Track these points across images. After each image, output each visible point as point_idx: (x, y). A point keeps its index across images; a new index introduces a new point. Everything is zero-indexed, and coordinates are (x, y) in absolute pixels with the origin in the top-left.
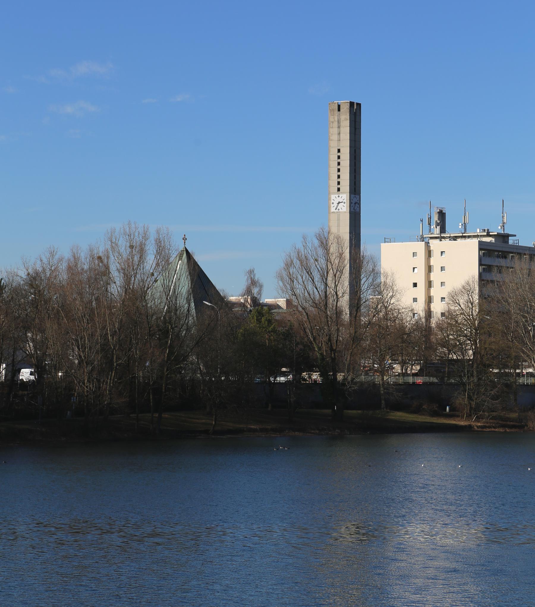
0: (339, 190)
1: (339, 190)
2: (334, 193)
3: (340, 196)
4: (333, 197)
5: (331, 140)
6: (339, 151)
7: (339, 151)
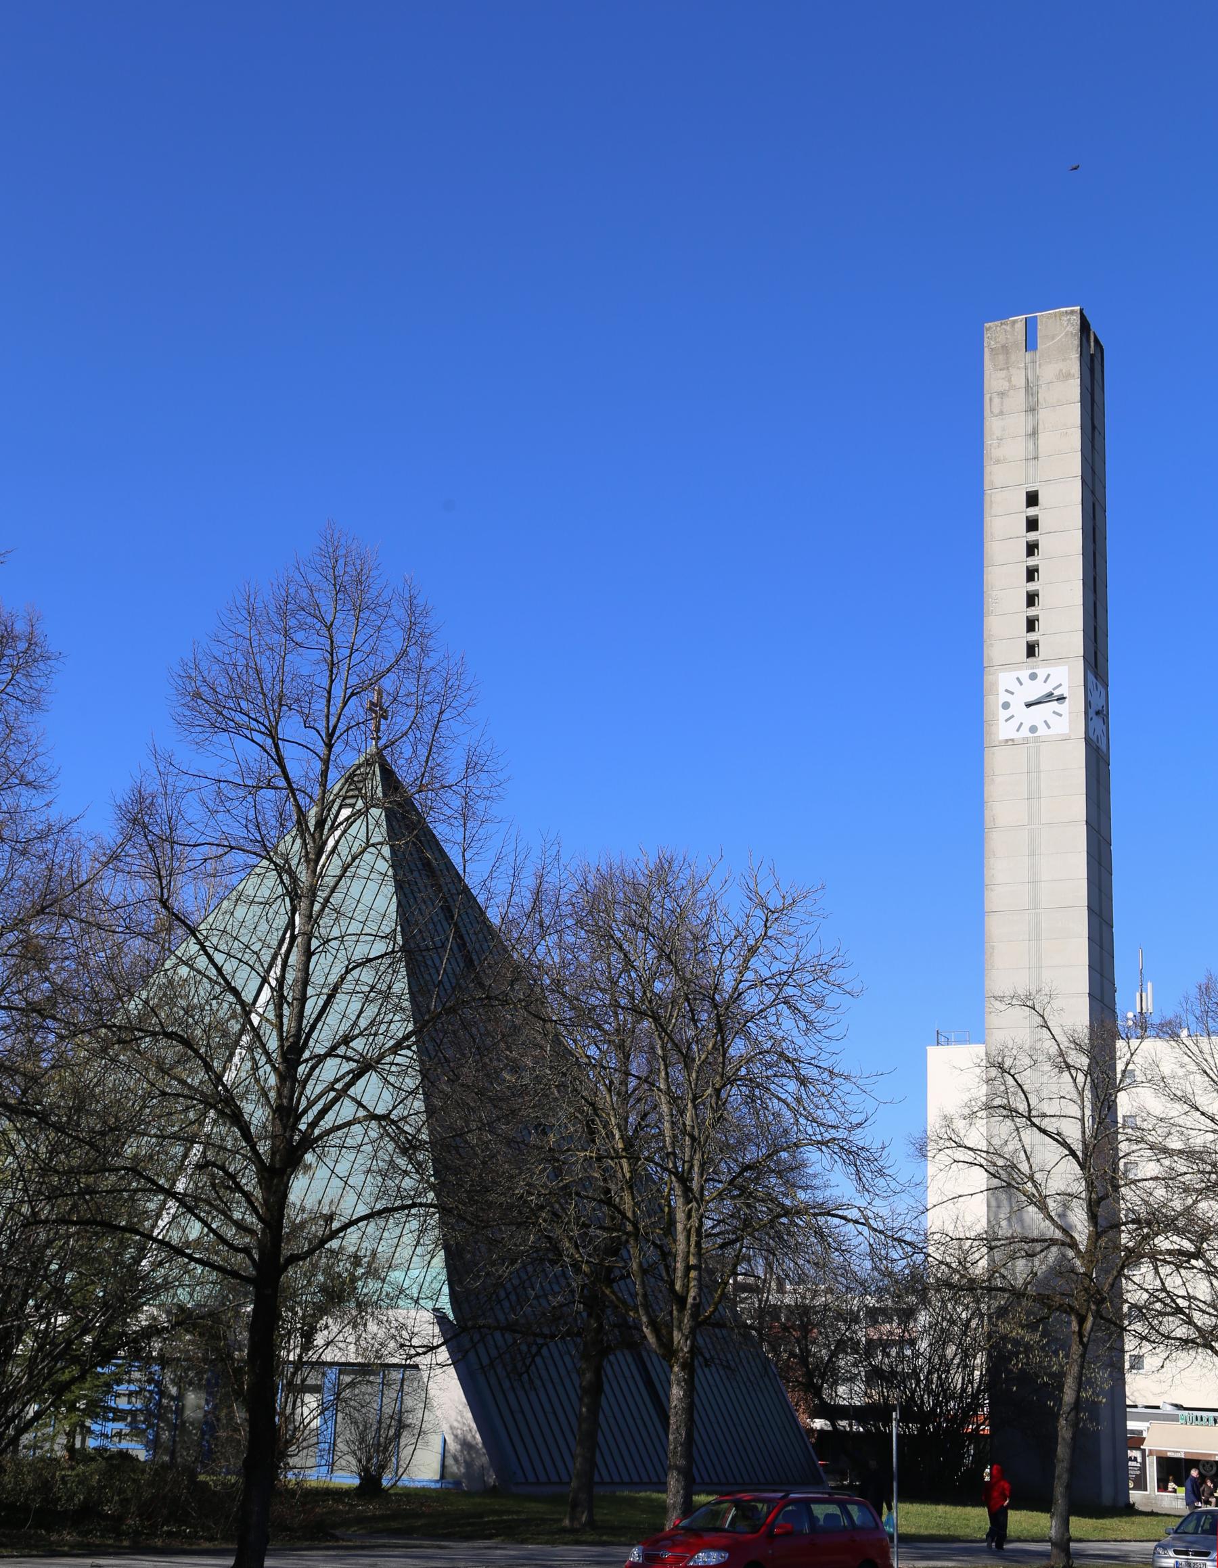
1: (1031, 650)
3: (1042, 673)
5: (998, 461)
6: (1032, 499)
7: (1032, 499)
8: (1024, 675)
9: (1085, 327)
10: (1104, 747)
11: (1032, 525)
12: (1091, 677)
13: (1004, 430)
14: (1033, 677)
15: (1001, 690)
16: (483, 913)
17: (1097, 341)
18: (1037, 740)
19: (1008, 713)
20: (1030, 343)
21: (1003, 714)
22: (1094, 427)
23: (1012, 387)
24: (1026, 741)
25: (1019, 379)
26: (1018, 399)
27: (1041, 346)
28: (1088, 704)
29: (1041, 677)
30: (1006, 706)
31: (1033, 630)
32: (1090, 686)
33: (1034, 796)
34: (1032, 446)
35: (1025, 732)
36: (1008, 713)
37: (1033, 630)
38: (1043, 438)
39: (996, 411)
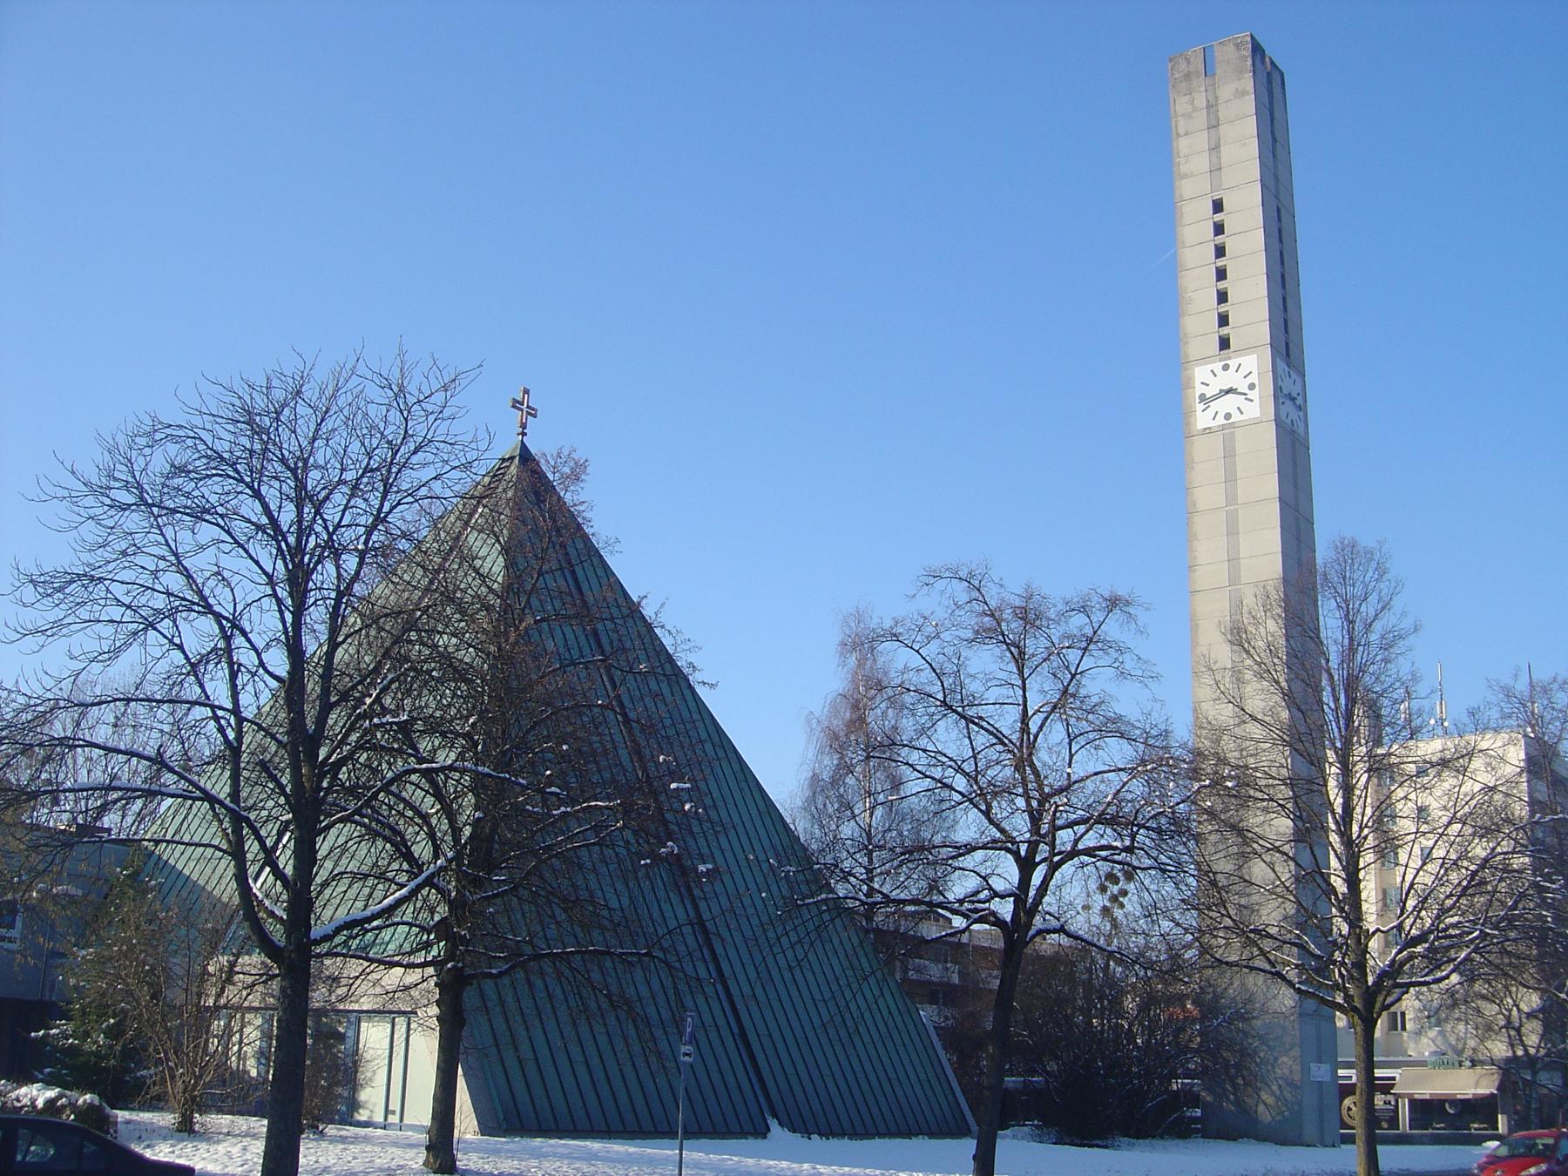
0: (1224, 343)
1: (1224, 343)
2: (1204, 360)
3: (1233, 363)
4: (1201, 373)
5: (1186, 176)
6: (1218, 206)
7: (1218, 206)
8: (1218, 367)
9: (1257, 49)
10: (1301, 430)
11: (1220, 251)
12: (1282, 365)
13: (1191, 151)
14: (1226, 368)
15: (1257, 401)
16: (506, 567)
17: (1272, 62)
18: (1232, 425)
19: (1250, 380)
20: (1208, 71)
21: (1254, 379)
22: (1275, 140)
23: (1195, 109)
24: (1223, 427)
25: (1201, 100)
26: (1201, 118)
27: (1219, 72)
28: (1278, 390)
29: (1233, 367)
30: (1252, 387)
31: (1227, 324)
32: (1280, 371)
33: (1230, 478)
34: (1214, 159)
35: (1221, 420)
36: (1250, 380)
37: (1227, 324)
38: (1225, 151)
39: (1181, 132)
